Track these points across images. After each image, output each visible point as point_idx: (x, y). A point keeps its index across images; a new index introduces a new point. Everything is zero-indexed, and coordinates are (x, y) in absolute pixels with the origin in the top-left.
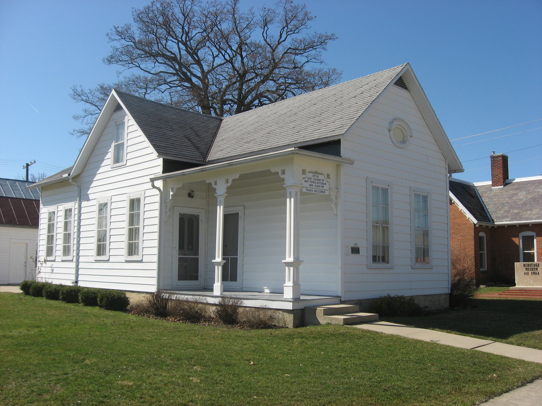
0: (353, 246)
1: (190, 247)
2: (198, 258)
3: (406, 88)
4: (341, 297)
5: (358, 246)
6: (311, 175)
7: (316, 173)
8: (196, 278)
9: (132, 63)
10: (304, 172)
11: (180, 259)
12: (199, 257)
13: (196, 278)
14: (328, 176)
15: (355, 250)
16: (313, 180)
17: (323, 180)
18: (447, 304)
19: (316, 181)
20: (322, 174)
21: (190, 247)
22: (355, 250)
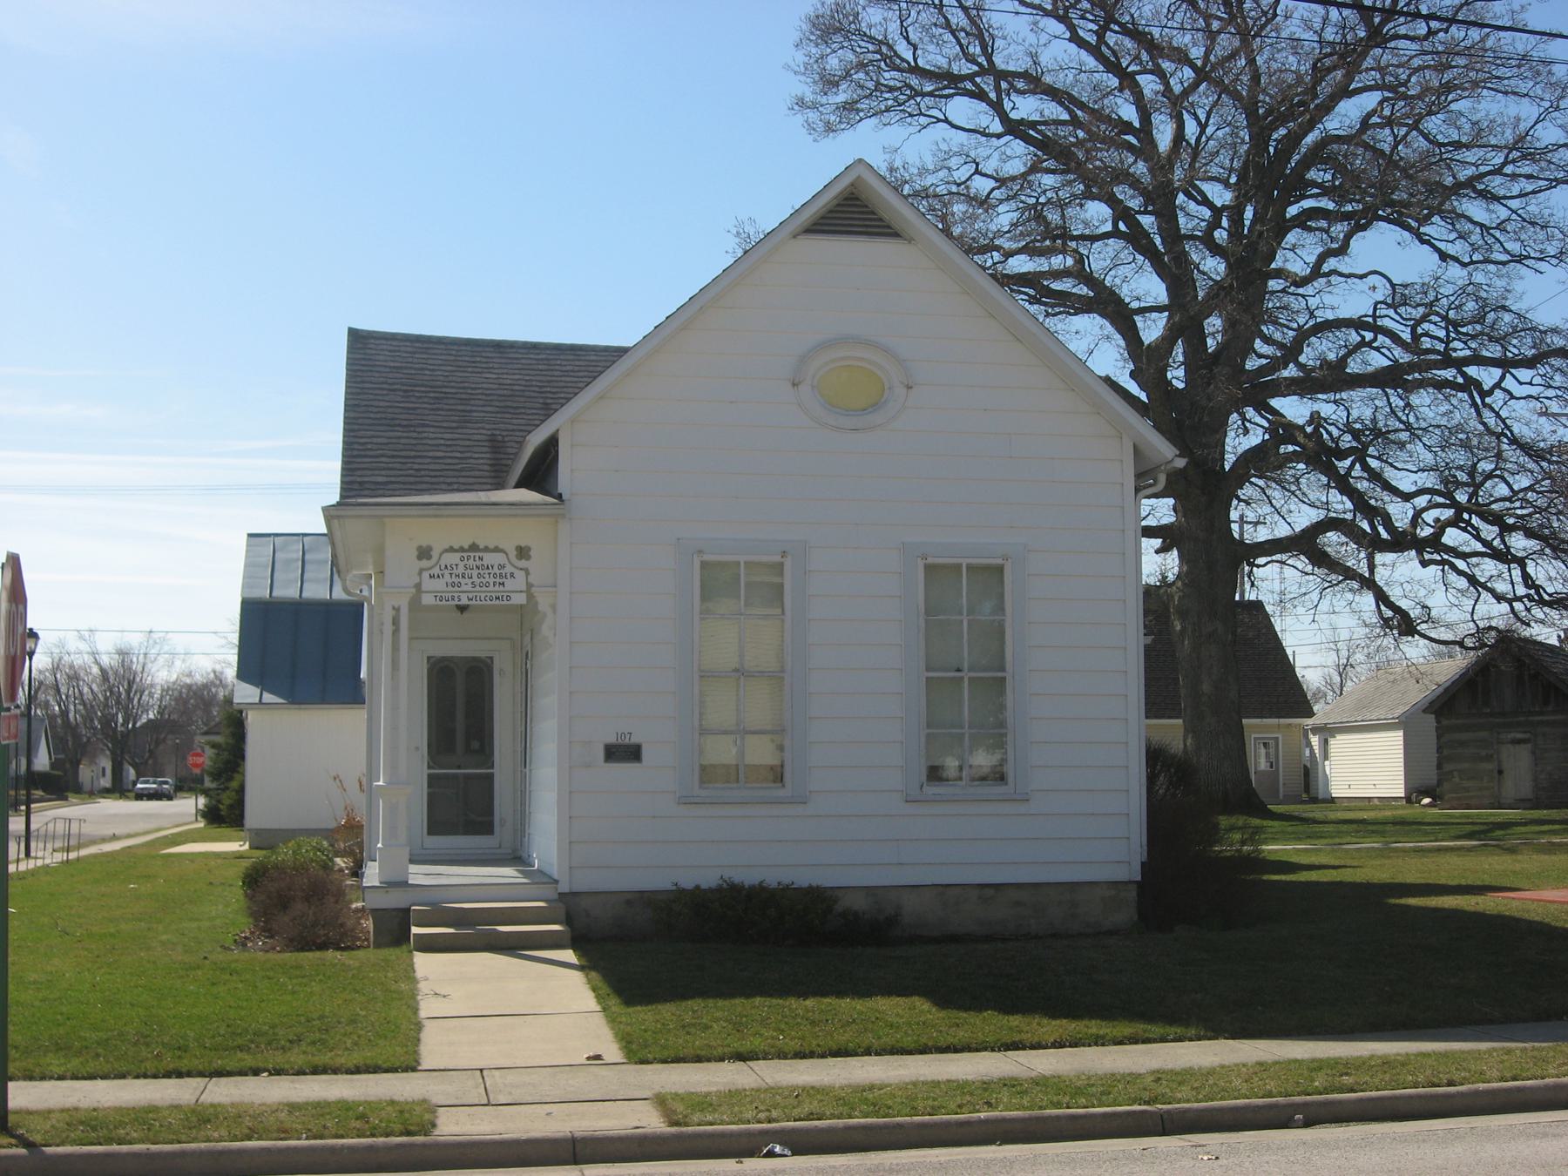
0: (612, 740)
1: (475, 745)
2: (490, 777)
3: (896, 235)
4: (556, 882)
5: (635, 740)
6: (453, 558)
7: (474, 548)
8: (486, 828)
9: (921, 114)
10: (424, 553)
11: (433, 781)
12: (496, 771)
13: (486, 828)
14: (523, 552)
15: (624, 752)
16: (461, 570)
17: (501, 567)
18: (1125, 915)
19: (475, 572)
20: (497, 550)
21: (475, 745)
22: (624, 752)
